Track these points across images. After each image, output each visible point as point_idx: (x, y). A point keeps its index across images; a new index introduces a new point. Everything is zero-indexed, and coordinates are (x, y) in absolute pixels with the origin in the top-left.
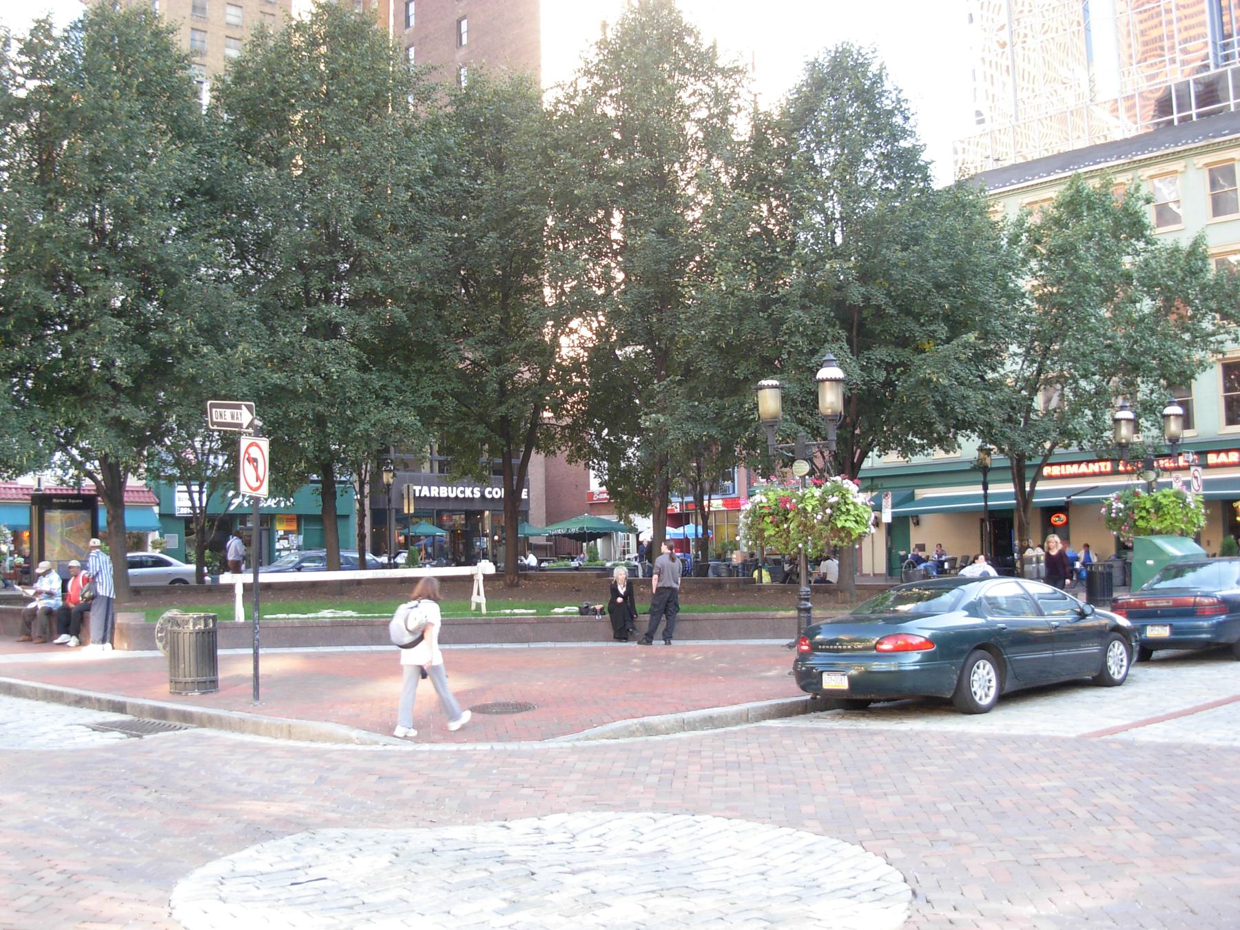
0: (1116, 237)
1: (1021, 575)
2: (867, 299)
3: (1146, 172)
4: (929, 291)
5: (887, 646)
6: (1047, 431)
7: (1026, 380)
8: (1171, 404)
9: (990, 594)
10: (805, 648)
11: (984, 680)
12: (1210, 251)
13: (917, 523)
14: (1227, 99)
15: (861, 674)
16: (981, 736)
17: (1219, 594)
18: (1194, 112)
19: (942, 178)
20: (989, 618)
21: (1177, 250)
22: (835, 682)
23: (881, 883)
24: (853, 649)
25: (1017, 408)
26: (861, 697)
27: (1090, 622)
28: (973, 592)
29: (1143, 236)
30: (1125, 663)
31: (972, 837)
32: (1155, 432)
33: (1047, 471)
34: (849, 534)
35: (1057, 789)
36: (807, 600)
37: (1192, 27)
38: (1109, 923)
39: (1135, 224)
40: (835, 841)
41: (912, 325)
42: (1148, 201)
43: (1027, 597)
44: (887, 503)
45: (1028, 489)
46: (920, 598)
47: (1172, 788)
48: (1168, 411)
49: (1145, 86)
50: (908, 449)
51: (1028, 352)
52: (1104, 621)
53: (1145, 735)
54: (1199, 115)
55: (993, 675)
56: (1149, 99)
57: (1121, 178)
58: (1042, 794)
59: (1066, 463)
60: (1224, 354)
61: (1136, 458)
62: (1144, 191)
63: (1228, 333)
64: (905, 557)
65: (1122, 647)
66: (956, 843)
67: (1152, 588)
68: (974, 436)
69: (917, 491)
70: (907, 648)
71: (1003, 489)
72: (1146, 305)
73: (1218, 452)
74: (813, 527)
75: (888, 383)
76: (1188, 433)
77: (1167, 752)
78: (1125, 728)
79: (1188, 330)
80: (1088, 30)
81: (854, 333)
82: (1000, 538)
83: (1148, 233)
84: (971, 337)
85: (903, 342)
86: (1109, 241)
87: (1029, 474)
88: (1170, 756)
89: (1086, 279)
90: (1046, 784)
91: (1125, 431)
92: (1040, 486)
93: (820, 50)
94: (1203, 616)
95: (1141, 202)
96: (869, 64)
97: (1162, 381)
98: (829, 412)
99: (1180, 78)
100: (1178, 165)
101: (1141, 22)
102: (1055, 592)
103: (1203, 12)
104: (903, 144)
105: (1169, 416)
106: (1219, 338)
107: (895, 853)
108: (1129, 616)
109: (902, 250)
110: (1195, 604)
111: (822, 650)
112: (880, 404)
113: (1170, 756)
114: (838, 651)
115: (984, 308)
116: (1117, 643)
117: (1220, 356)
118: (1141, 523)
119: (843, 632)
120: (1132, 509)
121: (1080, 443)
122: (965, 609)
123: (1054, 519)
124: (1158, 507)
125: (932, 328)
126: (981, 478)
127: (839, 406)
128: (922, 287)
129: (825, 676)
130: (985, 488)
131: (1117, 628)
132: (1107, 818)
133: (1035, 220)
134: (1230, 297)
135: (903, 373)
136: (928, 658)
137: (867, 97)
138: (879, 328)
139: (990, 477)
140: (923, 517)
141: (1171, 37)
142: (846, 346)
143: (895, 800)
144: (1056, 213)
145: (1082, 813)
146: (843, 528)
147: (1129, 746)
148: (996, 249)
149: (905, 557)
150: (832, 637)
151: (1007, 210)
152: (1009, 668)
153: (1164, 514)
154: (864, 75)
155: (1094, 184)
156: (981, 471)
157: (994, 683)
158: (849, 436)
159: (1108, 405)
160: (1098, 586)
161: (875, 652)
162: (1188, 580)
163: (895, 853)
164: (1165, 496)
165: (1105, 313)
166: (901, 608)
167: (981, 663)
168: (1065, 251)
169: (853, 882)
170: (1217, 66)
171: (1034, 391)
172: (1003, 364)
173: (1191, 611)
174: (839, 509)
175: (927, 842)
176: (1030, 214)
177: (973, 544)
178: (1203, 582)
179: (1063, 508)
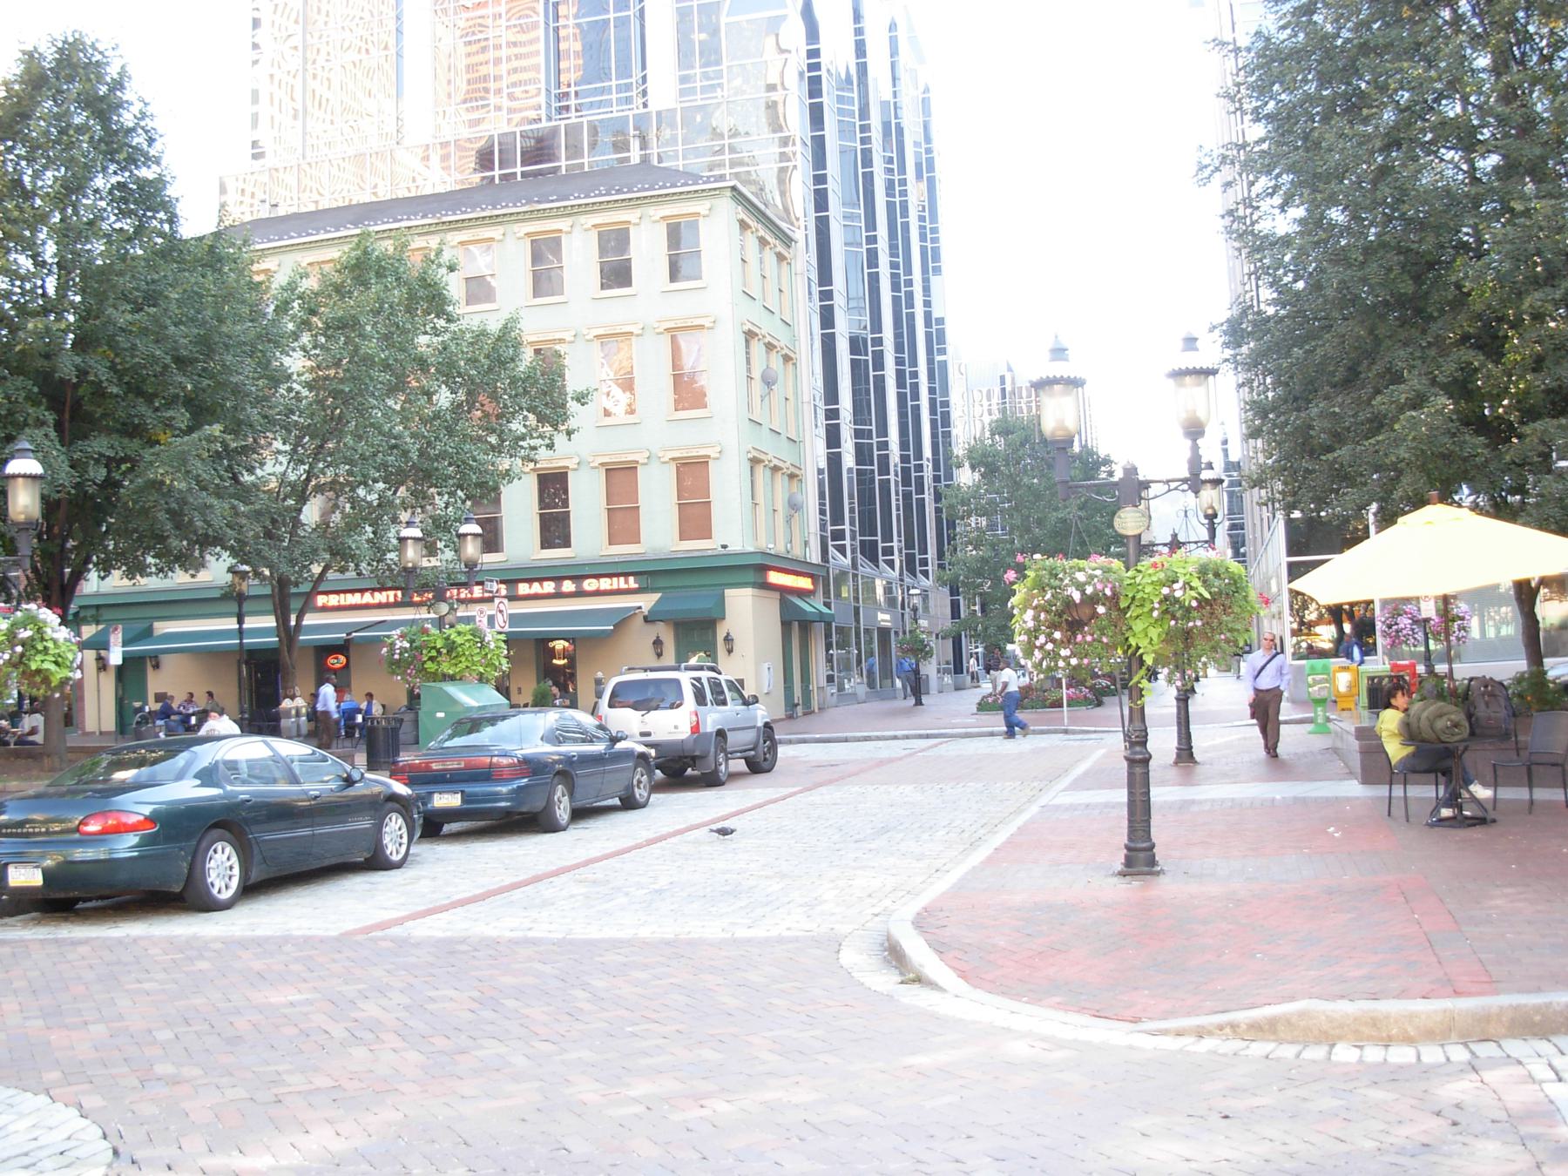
0: (410, 310)
1: (275, 731)
2: (82, 373)
3: (454, 238)
4: (166, 367)
5: (93, 827)
6: (315, 551)
7: (293, 485)
8: (467, 520)
9: (229, 757)
11: (222, 867)
12: (527, 338)
13: (157, 666)
14: (558, 159)
16: (216, 939)
17: (519, 753)
18: (519, 169)
19: (195, 223)
20: (229, 788)
21: (484, 333)
23: (72, 1144)
24: (47, 833)
25: (277, 521)
26: (62, 895)
27: (359, 789)
28: (206, 755)
29: (444, 312)
30: (405, 840)
31: (197, 1072)
32: (449, 554)
33: (321, 600)
34: (46, 681)
35: (309, 1002)
37: (524, 69)
38: (365, 1167)
40: (12, 1092)
41: (143, 409)
42: (452, 269)
43: (276, 759)
44: (116, 639)
45: (293, 623)
46: (140, 763)
47: (452, 993)
48: (464, 529)
49: (466, 133)
50: (136, 569)
51: (294, 451)
52: (377, 789)
53: (422, 929)
54: (524, 174)
55: (234, 860)
56: (467, 149)
57: (418, 242)
59: (345, 592)
61: (424, 588)
62: (446, 257)
63: (541, 437)
64: (141, 709)
65: (400, 820)
66: (175, 1081)
67: (442, 746)
68: (225, 554)
69: (157, 625)
71: (262, 622)
72: (444, 398)
73: (530, 581)
75: (110, 484)
76: (489, 558)
77: (448, 949)
78: (399, 922)
79: (494, 431)
80: (399, 55)
81: (67, 416)
82: (260, 688)
83: (450, 309)
84: (216, 429)
85: (132, 430)
86: (401, 318)
87: (295, 604)
88: (452, 953)
89: (368, 361)
90: (297, 997)
91: (412, 553)
92: (308, 620)
93: (44, 36)
94: (501, 780)
95: (443, 271)
96: (107, 64)
97: (460, 493)
98: (22, 518)
99: (507, 129)
100: (495, 232)
101: (469, 55)
102: (314, 753)
103: (538, 53)
105: (465, 535)
107: (92, 1101)
108: (410, 783)
109: (133, 312)
110: (491, 765)
112: (100, 512)
113: (452, 953)
114: (28, 835)
115: (237, 391)
116: (394, 816)
117: (532, 465)
118: (429, 665)
119: (34, 810)
120: (419, 649)
121: (357, 565)
122: (196, 777)
123: (331, 660)
124: (451, 647)
125: (170, 413)
126: (235, 609)
128: (156, 360)
129: (11, 870)
130: (240, 622)
131: (393, 797)
132: (369, 1036)
133: (311, 284)
134: (545, 394)
135: (131, 470)
136: (146, 842)
137: (103, 107)
138: (99, 411)
139: (246, 607)
140: (164, 659)
142: (53, 434)
143: (99, 1030)
144: (337, 278)
145: (338, 1031)
146: (38, 671)
147: (403, 943)
148: (256, 314)
149: (141, 709)
150: (19, 817)
151: (281, 269)
152: (256, 851)
154: (100, 78)
155: (388, 246)
156: (234, 600)
157: (236, 871)
158: (56, 550)
159: (395, 520)
160: (381, 742)
161: (77, 836)
162: (485, 736)
163: (92, 1101)
164: (459, 633)
165: (395, 403)
166: (120, 776)
167: (219, 846)
168: (345, 325)
169: (34, 1144)
170: (550, 119)
171: (303, 499)
172: (262, 464)
173: (487, 774)
174: (33, 647)
175: (136, 1083)
176: (307, 276)
177: (229, 692)
179: (342, 648)
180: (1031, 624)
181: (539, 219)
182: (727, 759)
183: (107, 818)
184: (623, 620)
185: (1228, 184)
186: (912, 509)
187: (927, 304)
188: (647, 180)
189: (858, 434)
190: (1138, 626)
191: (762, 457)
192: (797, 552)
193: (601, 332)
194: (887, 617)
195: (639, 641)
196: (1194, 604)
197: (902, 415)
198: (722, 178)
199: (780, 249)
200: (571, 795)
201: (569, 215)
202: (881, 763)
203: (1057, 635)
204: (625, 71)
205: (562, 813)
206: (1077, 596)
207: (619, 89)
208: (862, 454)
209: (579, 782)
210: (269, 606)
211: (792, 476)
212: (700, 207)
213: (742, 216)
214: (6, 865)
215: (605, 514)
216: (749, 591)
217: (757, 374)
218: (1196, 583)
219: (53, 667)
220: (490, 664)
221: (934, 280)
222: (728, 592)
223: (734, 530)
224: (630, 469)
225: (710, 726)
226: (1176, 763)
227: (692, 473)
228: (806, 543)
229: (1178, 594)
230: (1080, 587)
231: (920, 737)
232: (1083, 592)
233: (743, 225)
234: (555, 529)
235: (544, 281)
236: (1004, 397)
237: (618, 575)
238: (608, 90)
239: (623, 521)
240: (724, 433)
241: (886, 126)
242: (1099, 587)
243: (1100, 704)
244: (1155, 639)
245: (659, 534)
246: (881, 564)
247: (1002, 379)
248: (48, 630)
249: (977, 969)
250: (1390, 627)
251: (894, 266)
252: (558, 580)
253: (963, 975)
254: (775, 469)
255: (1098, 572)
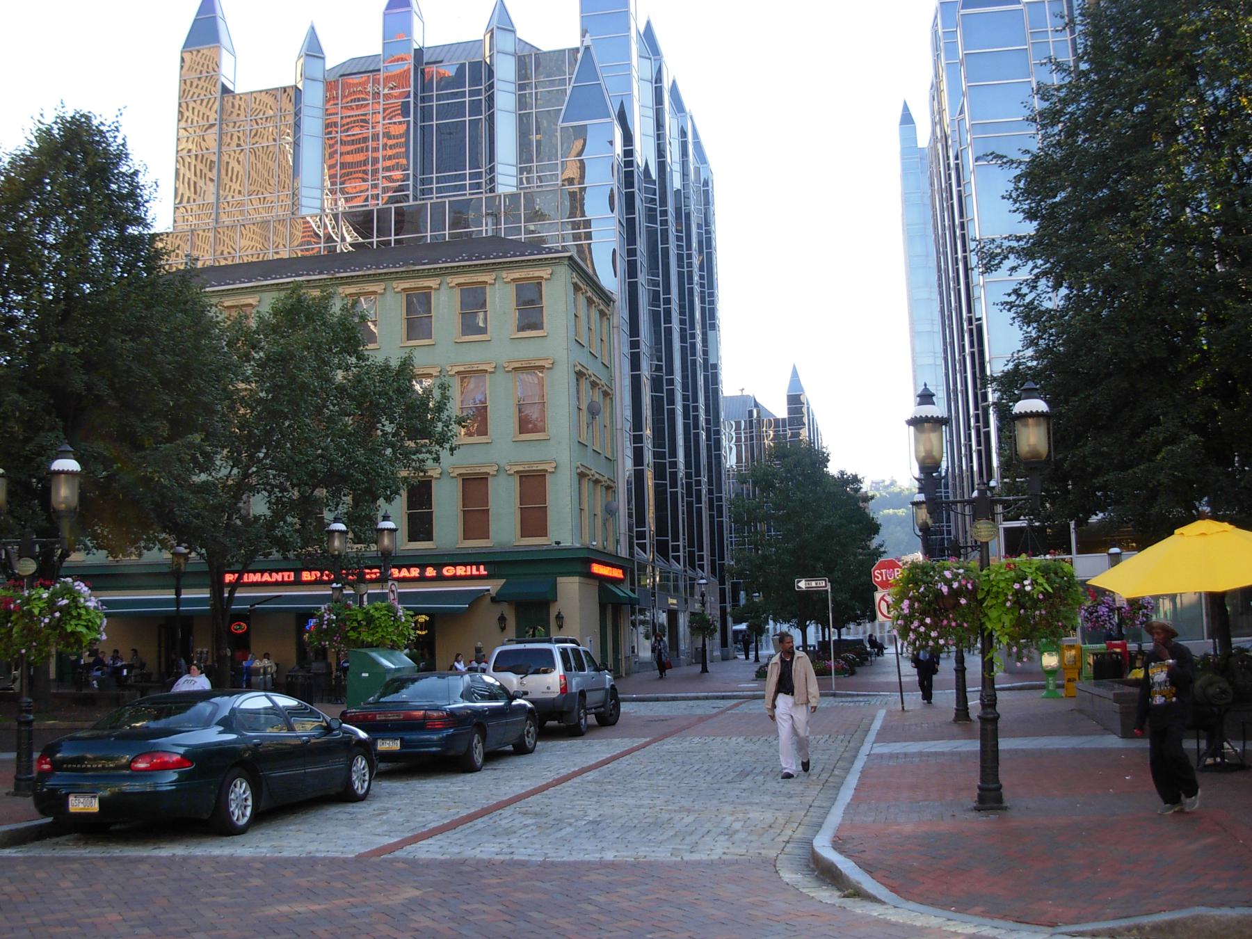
2: (89, 388)
10: (46, 767)
15: (113, 794)
22: (82, 804)
29: (356, 352)
30: (367, 778)
36: (29, 712)
39: (350, 339)
53: (427, 850)
58: (353, 921)
60: (425, 472)
63: (430, 452)
70: (165, 766)
74: (40, 631)
77: (454, 868)
84: (197, 438)
100: (378, 287)
104: (133, 230)
106: (421, 456)
111: (67, 770)
120: (344, 621)
122: (218, 724)
124: (370, 620)
127: (74, 501)
129: (72, 799)
130: (178, 594)
141: (375, 161)
146: (73, 633)
153: (376, 627)
156: (176, 577)
157: (250, 802)
162: (404, 695)
164: (376, 609)
170: (415, 199)
173: (421, 725)
174: (70, 614)
178: (423, 695)
180: (906, 611)
181: (413, 278)
182: (586, 715)
183: (153, 757)
184: (476, 599)
185: (1013, 269)
186: (693, 515)
187: (705, 353)
188: (499, 252)
189: (656, 455)
190: (993, 614)
191: (588, 472)
192: (611, 548)
193: (461, 369)
194: (675, 601)
195: (488, 616)
196: (1041, 597)
197: (687, 440)
198: (565, 249)
199: (602, 307)
200: (484, 739)
201: (438, 275)
202: (702, 719)
203: (928, 621)
204: (475, 164)
205: (478, 757)
206: (945, 589)
207: (472, 176)
208: (659, 472)
209: (489, 731)
210: (208, 580)
211: (608, 488)
212: (544, 273)
213: (576, 280)
214: (67, 795)
215: (461, 515)
216: (576, 579)
217: (584, 406)
218: (1041, 580)
219: (84, 630)
220: (401, 634)
221: (710, 333)
222: (560, 580)
223: (564, 530)
224: (482, 479)
225: (574, 689)
226: (955, 721)
227: (532, 484)
228: (618, 542)
229: (1028, 588)
230: (948, 582)
231: (717, 698)
232: (950, 587)
233: (576, 288)
234: (420, 526)
235: (417, 325)
236: (751, 427)
237: (471, 564)
238: (463, 177)
239: (475, 518)
240: (559, 451)
241: (678, 211)
242: (963, 582)
243: (853, 673)
244: (1007, 624)
245: (505, 530)
246: (672, 560)
247: (751, 412)
248: (82, 600)
249: (906, 884)
250: (1091, 614)
251: (682, 322)
252: (422, 567)
253: (893, 889)
254: (597, 482)
255: (961, 571)
